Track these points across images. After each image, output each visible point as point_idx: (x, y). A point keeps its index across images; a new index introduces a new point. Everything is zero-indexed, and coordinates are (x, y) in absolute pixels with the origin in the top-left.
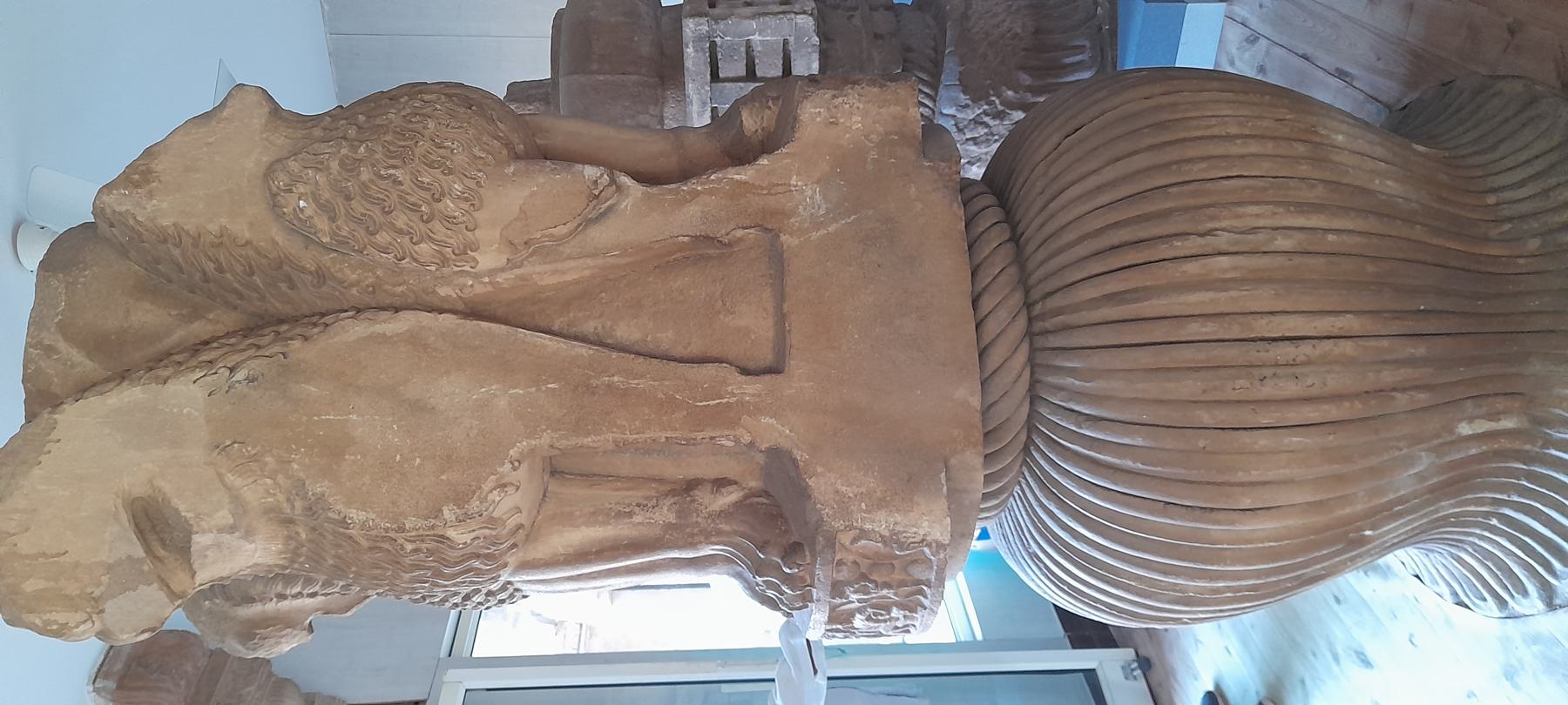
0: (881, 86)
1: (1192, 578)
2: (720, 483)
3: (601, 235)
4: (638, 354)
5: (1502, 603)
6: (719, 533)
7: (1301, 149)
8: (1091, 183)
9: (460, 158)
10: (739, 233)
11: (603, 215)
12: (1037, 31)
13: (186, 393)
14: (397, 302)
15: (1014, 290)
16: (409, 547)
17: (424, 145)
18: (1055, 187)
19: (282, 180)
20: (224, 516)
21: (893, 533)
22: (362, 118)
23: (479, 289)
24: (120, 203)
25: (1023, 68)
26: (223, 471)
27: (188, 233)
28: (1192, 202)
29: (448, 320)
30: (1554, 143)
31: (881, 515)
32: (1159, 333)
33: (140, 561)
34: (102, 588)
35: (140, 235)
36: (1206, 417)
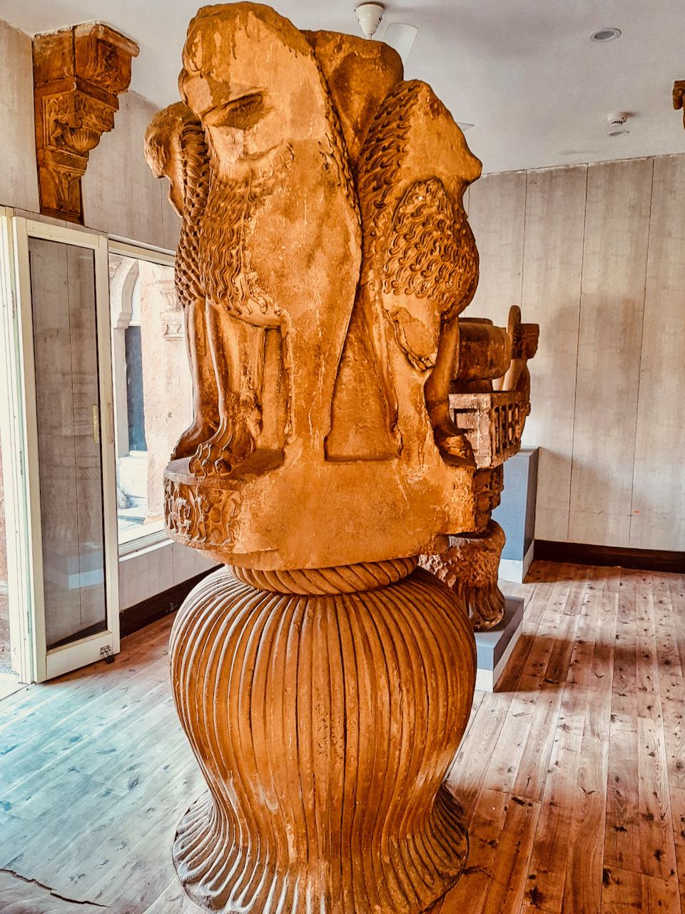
0: (473, 512)
1: (208, 686)
2: (260, 424)
3: (399, 362)
4: (336, 381)
5: (182, 857)
6: (234, 424)
7: (440, 736)
8: (423, 625)
9: (443, 286)
10: (399, 436)
11: (409, 362)
12: (477, 589)
13: (320, 129)
14: (366, 248)
15: (366, 584)
16: (234, 252)
17: (450, 266)
18: (419, 606)
19: (433, 187)
20: (253, 149)
21: (239, 522)
22: (464, 232)
23: (372, 294)
24: (423, 95)
25: (457, 582)
26: (278, 149)
27: (406, 133)
28: (416, 679)
29: (356, 276)
30: (437, 867)
31: (249, 516)
32: (349, 664)
33: (227, 98)
34: (215, 78)
35: (405, 106)
36: (304, 690)
